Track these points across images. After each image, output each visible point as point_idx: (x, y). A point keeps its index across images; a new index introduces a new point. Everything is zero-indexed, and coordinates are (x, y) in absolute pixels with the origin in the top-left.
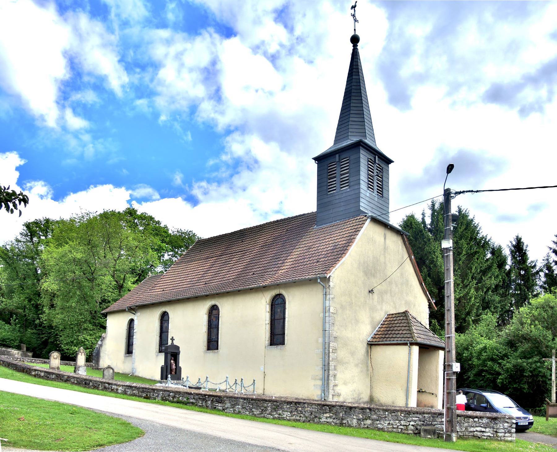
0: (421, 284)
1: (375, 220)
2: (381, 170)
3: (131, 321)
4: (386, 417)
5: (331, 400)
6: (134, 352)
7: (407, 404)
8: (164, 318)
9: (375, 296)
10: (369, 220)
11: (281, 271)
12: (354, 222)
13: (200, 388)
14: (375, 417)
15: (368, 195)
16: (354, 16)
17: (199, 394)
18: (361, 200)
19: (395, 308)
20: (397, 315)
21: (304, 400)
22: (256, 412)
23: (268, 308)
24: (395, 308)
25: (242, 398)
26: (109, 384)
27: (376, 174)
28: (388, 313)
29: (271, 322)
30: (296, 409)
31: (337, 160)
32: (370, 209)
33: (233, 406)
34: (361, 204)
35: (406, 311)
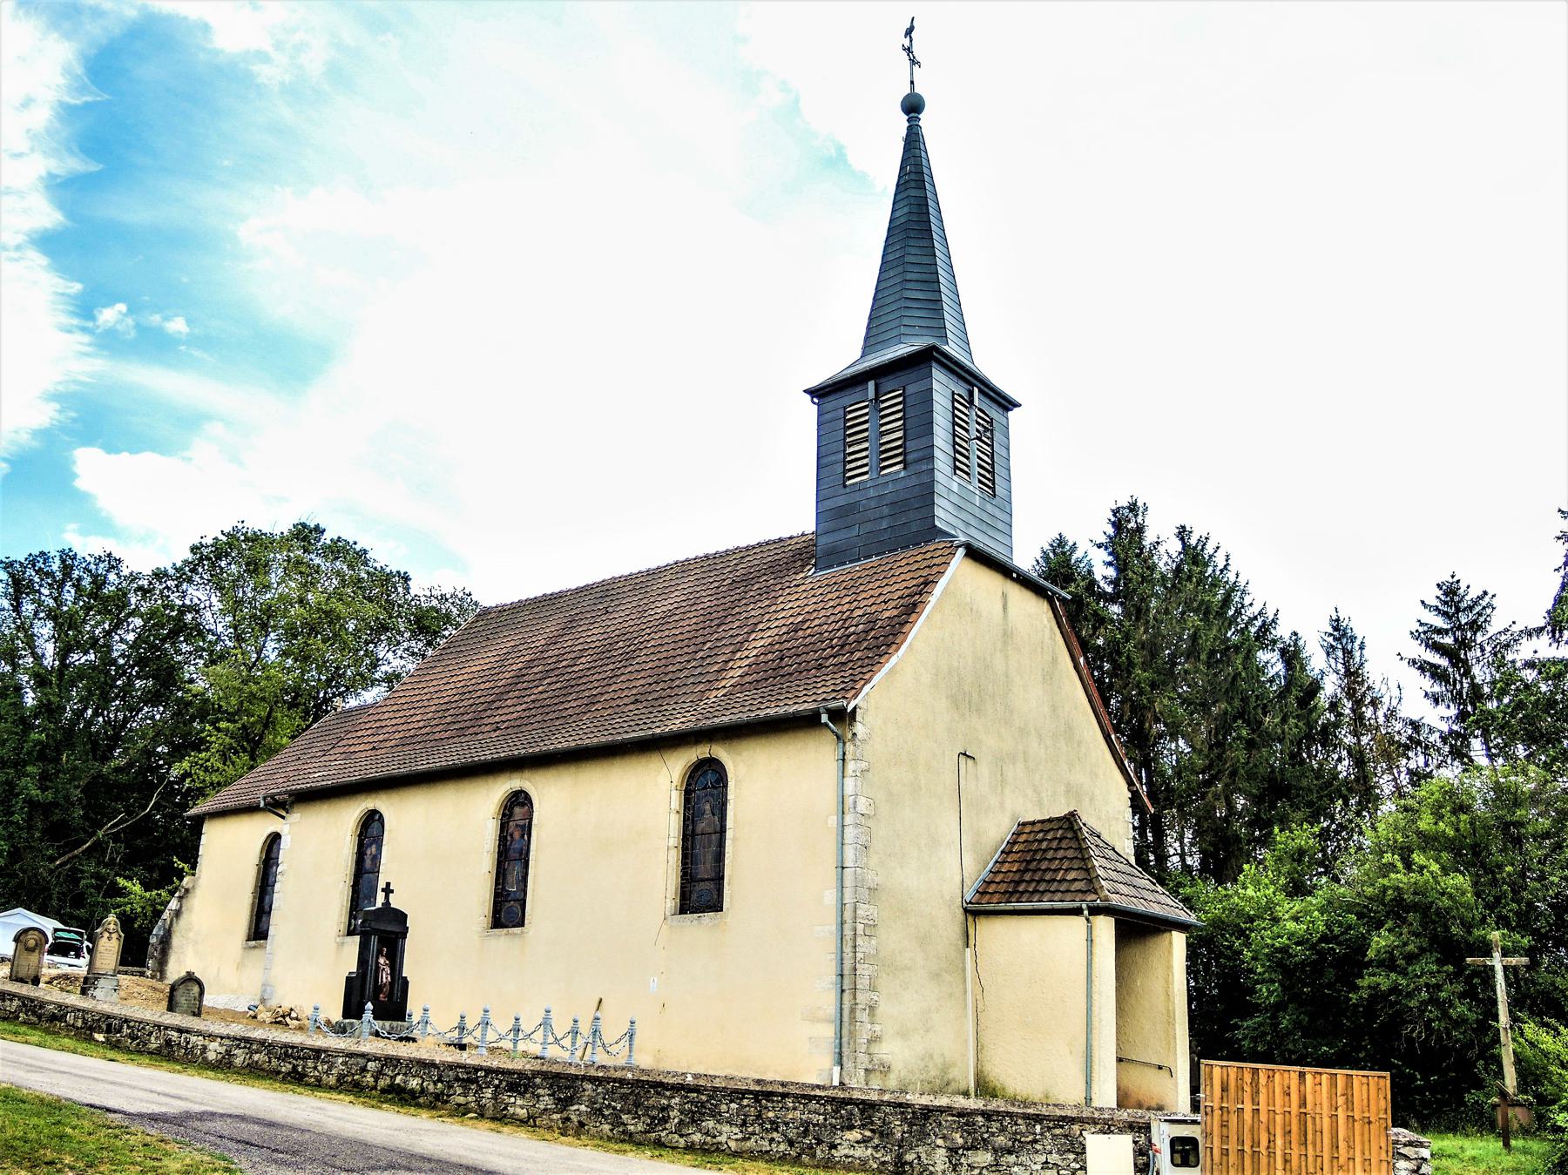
0: (1107, 738)
1: (976, 555)
2: (988, 429)
3: (274, 840)
4: (1035, 1141)
5: (861, 1086)
6: (270, 933)
7: (1088, 1100)
8: (370, 830)
9: (984, 769)
10: (961, 552)
11: (714, 693)
12: (919, 558)
13: (462, 1047)
14: (1001, 1140)
15: (955, 488)
16: (909, 50)
17: (460, 1066)
18: (937, 500)
19: (1040, 803)
20: (1048, 826)
21: (783, 1085)
22: (635, 1126)
23: (676, 800)
24: (1040, 803)
25: (592, 1080)
26: (180, 1031)
27: (974, 434)
28: (1021, 820)
29: (685, 839)
30: (759, 1116)
31: (871, 394)
32: (961, 525)
33: (564, 1104)
34: (938, 512)
35: (1072, 814)
